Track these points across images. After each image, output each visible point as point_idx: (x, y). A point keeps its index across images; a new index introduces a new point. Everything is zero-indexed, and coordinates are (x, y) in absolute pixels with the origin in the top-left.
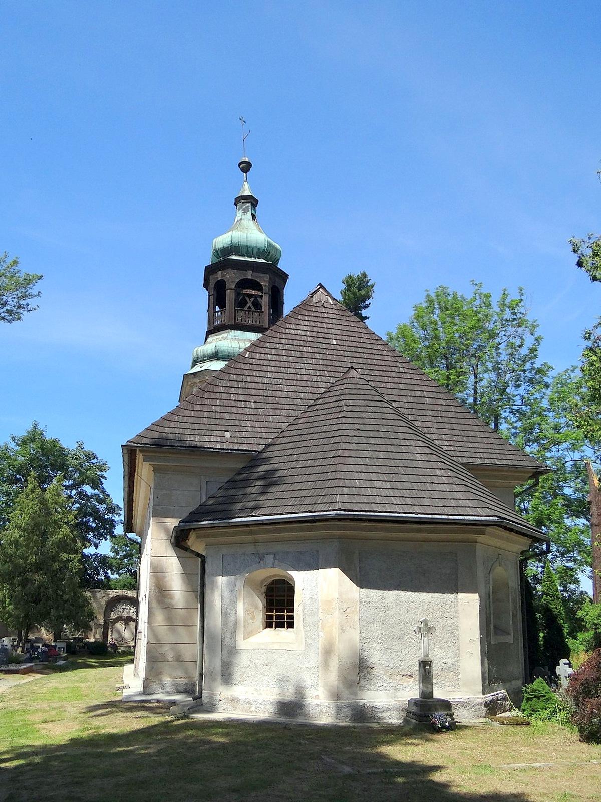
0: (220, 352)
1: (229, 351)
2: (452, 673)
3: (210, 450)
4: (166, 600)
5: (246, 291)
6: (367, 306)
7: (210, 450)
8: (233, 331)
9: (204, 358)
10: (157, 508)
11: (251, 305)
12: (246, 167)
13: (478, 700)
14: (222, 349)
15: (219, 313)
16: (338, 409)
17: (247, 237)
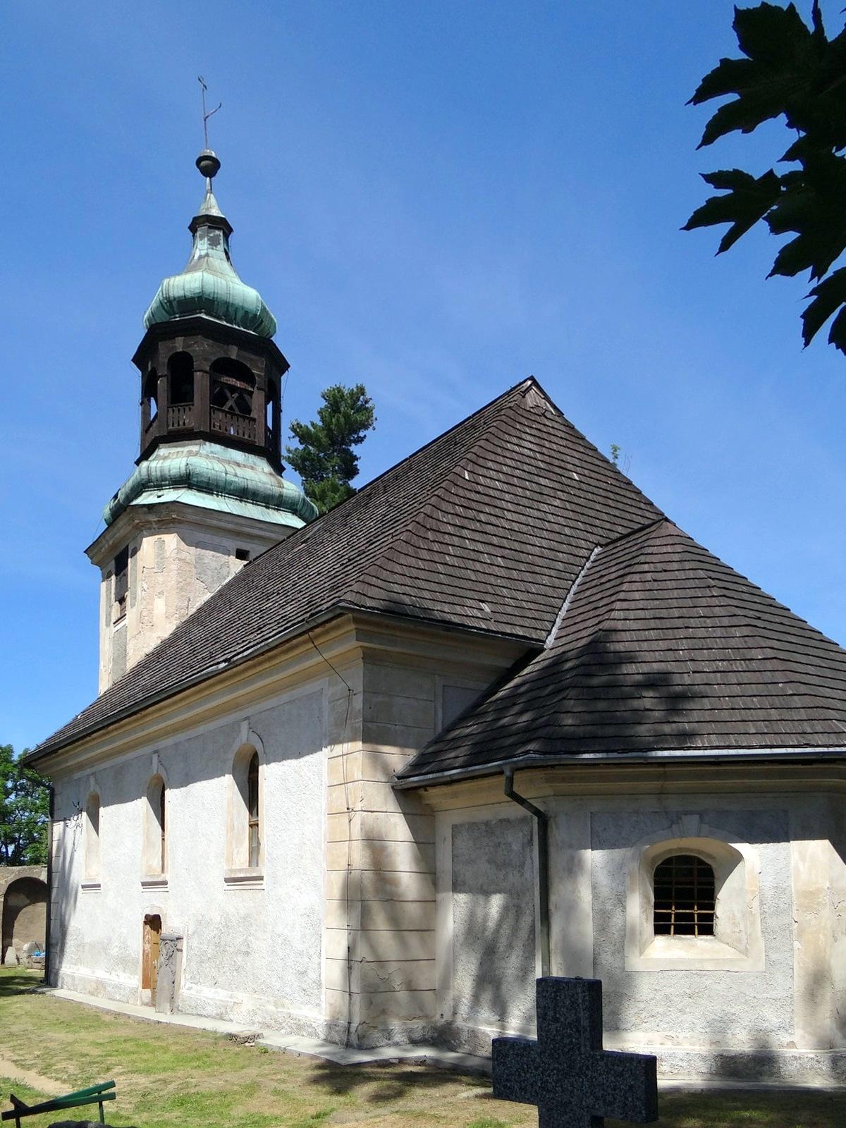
0: (194, 475)
1: (210, 475)
3: (472, 630)
4: (388, 887)
5: (225, 379)
7: (472, 630)
8: (207, 443)
9: (162, 481)
10: (370, 725)
11: (234, 406)
12: (209, 167)
14: (198, 470)
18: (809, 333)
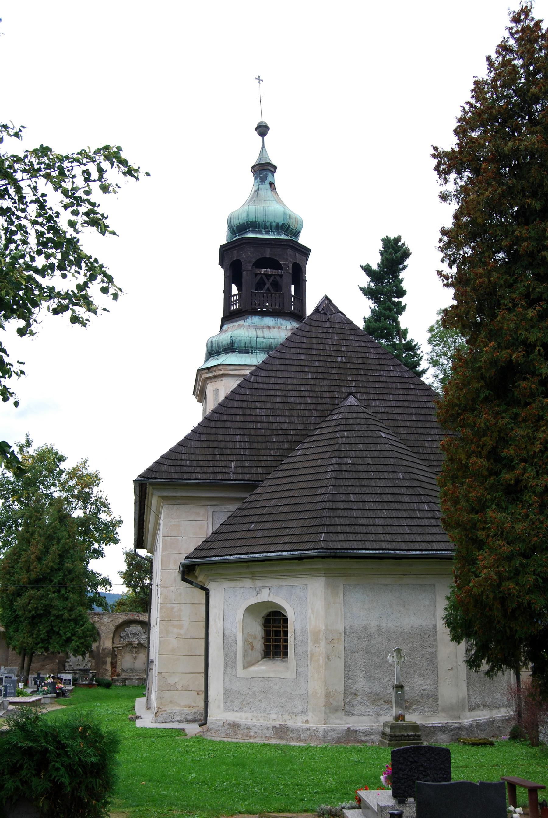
2: (431, 699)
6: (404, 268)
10: (166, 538)
13: (456, 725)
15: (235, 297)
16: (332, 442)
17: (264, 210)
18: (405, 305)
